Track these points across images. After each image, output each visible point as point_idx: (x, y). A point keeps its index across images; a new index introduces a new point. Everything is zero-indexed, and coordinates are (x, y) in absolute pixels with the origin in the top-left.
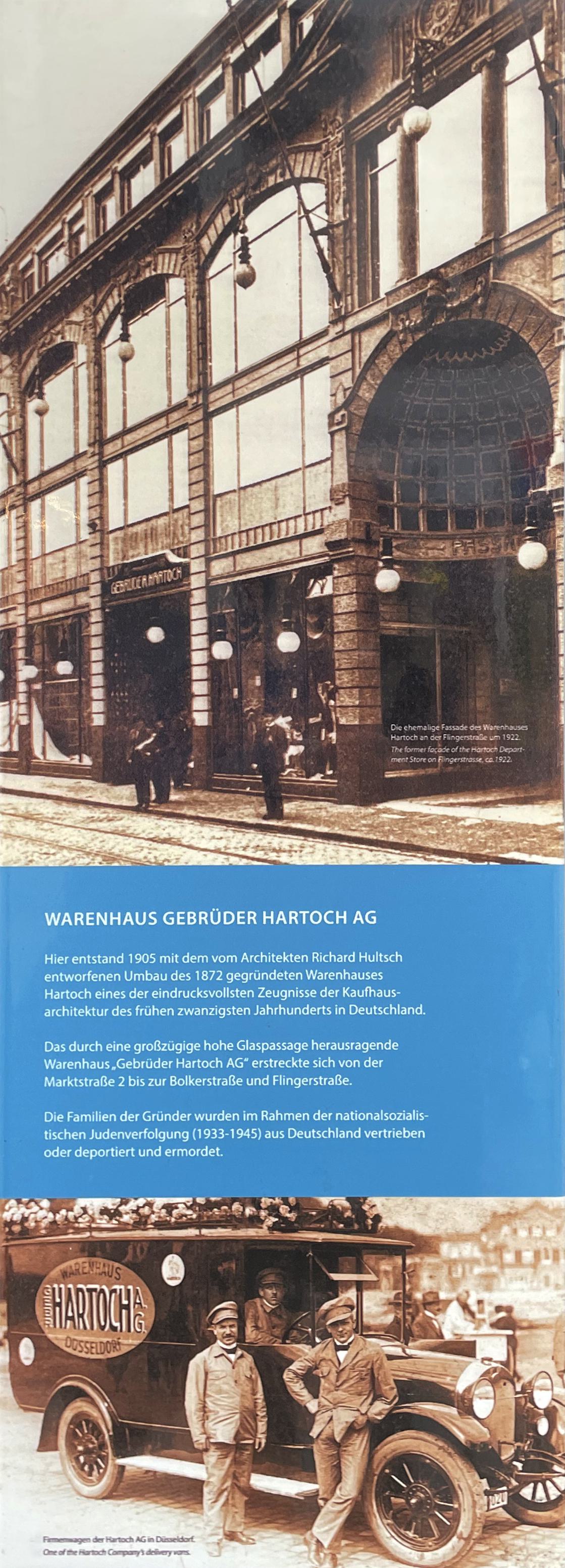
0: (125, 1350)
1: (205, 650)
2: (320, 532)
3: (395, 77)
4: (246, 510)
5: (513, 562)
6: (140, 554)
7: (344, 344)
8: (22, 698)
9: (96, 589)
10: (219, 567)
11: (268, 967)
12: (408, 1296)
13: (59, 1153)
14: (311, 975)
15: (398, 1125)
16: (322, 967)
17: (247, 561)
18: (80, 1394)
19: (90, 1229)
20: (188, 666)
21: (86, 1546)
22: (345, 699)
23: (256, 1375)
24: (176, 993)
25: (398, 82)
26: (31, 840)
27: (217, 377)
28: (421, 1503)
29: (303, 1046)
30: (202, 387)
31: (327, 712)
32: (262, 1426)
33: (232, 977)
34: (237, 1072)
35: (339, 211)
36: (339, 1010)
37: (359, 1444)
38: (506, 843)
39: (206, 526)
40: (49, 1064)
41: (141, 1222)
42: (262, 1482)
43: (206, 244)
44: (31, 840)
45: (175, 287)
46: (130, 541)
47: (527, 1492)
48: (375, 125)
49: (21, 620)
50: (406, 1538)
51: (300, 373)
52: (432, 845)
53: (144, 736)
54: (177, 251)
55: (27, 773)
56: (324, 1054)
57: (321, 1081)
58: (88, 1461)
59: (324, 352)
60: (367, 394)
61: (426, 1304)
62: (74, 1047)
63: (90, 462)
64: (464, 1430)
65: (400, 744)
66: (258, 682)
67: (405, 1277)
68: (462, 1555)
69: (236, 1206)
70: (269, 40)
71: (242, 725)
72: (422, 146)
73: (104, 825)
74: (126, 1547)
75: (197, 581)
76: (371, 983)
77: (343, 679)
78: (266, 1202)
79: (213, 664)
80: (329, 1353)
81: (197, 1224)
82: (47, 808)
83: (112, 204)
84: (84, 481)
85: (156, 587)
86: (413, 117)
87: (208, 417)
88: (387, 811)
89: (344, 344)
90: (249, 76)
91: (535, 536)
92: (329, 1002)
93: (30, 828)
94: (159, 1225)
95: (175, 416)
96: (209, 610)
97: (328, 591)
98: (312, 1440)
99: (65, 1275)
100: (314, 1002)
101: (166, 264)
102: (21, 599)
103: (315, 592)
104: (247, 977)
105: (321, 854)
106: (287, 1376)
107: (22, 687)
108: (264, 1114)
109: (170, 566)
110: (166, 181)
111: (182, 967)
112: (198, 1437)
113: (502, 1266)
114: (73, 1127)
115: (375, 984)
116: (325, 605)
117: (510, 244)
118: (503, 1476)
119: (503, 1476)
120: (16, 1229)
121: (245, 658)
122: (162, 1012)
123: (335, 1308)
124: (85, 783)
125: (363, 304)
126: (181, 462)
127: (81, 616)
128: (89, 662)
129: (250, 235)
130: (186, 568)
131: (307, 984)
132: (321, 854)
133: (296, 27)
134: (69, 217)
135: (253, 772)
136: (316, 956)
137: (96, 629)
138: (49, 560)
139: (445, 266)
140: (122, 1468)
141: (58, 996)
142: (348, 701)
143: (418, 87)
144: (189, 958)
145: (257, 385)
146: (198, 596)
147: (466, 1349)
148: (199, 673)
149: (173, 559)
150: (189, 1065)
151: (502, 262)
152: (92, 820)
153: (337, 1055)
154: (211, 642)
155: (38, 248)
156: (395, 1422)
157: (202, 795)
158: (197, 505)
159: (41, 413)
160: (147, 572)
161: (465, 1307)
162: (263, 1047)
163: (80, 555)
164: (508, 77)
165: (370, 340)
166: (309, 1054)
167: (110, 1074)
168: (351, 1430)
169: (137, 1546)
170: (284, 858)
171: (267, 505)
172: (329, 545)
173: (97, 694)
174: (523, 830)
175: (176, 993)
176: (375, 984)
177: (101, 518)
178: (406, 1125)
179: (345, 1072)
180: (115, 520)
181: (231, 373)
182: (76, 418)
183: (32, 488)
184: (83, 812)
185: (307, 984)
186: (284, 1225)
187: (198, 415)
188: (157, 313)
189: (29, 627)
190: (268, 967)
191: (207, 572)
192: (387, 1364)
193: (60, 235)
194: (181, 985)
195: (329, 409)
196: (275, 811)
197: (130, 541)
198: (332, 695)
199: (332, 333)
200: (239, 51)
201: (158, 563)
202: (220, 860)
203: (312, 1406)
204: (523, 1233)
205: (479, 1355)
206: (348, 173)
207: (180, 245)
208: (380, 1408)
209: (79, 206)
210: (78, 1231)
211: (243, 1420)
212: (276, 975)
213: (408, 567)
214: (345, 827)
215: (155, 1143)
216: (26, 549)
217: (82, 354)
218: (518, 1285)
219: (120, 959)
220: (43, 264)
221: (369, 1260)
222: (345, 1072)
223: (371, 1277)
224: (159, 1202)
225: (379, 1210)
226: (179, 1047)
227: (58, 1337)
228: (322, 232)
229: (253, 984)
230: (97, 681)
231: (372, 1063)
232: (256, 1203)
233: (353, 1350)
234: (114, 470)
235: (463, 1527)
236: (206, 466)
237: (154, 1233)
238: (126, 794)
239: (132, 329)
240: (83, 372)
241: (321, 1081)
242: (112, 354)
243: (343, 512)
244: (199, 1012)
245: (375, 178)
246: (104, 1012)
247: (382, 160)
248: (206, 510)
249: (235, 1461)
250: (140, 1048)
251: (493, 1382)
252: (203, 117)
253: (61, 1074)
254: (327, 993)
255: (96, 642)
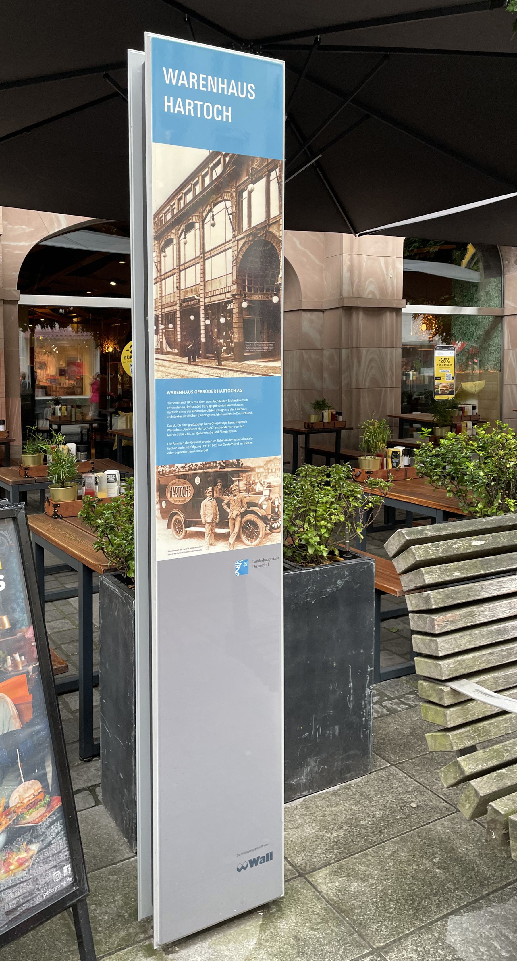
0: (187, 501)
1: (204, 322)
2: (230, 292)
3: (247, 176)
4: (213, 286)
5: (271, 301)
6: (188, 296)
7: (235, 243)
8: (161, 334)
9: (178, 305)
10: (207, 300)
11: (218, 404)
12: (249, 482)
13: (171, 453)
14: (228, 405)
15: (247, 441)
16: (230, 403)
17: (214, 299)
18: (177, 514)
19: (178, 472)
20: (200, 326)
21: (178, 552)
22: (236, 335)
23: (216, 505)
24: (197, 411)
25: (247, 177)
26: (163, 372)
27: (206, 250)
28: (252, 531)
29: (226, 423)
30: (203, 253)
31: (231, 338)
32: (218, 517)
33: (210, 406)
34: (212, 430)
35: (234, 209)
36: (234, 414)
37: (239, 518)
38: (270, 371)
39: (204, 289)
40: (168, 430)
41: (190, 469)
42: (218, 531)
43: (204, 215)
44: (163, 372)
45: (197, 225)
46: (186, 292)
47: (273, 526)
48: (242, 188)
49: (160, 313)
50: (248, 540)
51: (226, 250)
52: (254, 372)
53: (190, 344)
54: (197, 216)
55: (162, 354)
56: (231, 425)
57: (230, 431)
58: (179, 530)
59: (231, 245)
60: (240, 257)
61: (253, 484)
62: (174, 426)
63: (177, 271)
64: (261, 513)
65: (248, 347)
66: (216, 330)
67: (248, 477)
68: (260, 543)
69: (212, 463)
70: (218, 163)
71: (212, 342)
72: (252, 194)
73: (181, 368)
74: (187, 550)
75: (202, 304)
76: (241, 407)
77: (235, 330)
78: (218, 462)
79: (206, 326)
80: (232, 498)
81: (203, 469)
82: (167, 363)
83: (182, 202)
84: (175, 276)
85: (192, 305)
86: (251, 186)
87: (204, 260)
88: (245, 364)
89: (235, 243)
90: (214, 171)
91: (276, 295)
92: (232, 412)
93: (163, 369)
94: (195, 470)
95: (197, 260)
96: (205, 311)
97: (232, 307)
98: (229, 519)
99: (173, 484)
100: (229, 412)
101: (195, 219)
102: (160, 307)
103: (229, 308)
104: (214, 406)
105: (230, 375)
106: (223, 504)
107: (160, 331)
108: (218, 440)
109: (196, 299)
110: (195, 197)
111: (199, 404)
112: (204, 522)
113: (269, 473)
114: (174, 446)
115: (242, 407)
116: (231, 311)
117: (271, 221)
118: (268, 522)
119: (268, 522)
120: (161, 473)
121: (213, 324)
122: (195, 416)
123: (233, 487)
124: (176, 357)
125: (240, 234)
126: (198, 272)
127: (175, 312)
128: (177, 324)
129: (214, 213)
130: (199, 300)
131: (227, 407)
132: (230, 375)
133: (225, 160)
134: (172, 204)
135: (215, 354)
136: (229, 401)
137: (178, 316)
138: (167, 297)
139: (257, 225)
140: (186, 531)
141: (170, 412)
142: (236, 336)
143: (252, 179)
144: (201, 402)
145: (216, 253)
146: (202, 308)
147: (261, 493)
148: (202, 328)
149: (196, 297)
150: (201, 429)
151: (269, 225)
152: (178, 366)
153: (234, 425)
154: (205, 320)
155: (164, 212)
156: (247, 512)
157: (203, 360)
158: (202, 283)
159: (165, 257)
160: (191, 301)
161: (261, 483)
162: (217, 424)
163: (174, 296)
164: (271, 179)
165: (241, 243)
166: (228, 425)
167: (182, 432)
168: (237, 515)
169: (190, 550)
170: (222, 376)
171: (218, 284)
172: (232, 295)
173: (179, 333)
174: (273, 368)
175: (197, 411)
176: (242, 407)
177: (179, 286)
178: (248, 441)
179: (235, 429)
180: (183, 287)
181: (210, 249)
182: (173, 259)
183: (163, 277)
184: (176, 364)
185: (227, 407)
186: (222, 467)
187: (202, 260)
188: (193, 232)
189: (162, 315)
190: (218, 404)
191: (204, 301)
192: (245, 499)
193: (169, 209)
194: (199, 409)
195: (232, 260)
196: (220, 364)
197: (186, 292)
198: (232, 334)
199: (233, 241)
200: (212, 165)
201: (193, 299)
202: (207, 377)
203: (229, 511)
204: (273, 465)
205: (264, 494)
206: (236, 199)
207: (198, 214)
208: (243, 509)
209: (197, 179)
210: (176, 473)
211: (214, 515)
212: (220, 406)
213: (249, 301)
214: (235, 368)
215: (193, 449)
216: (161, 294)
217: (175, 241)
218: (272, 477)
219: (185, 403)
220: (165, 216)
221: (241, 474)
222: (235, 429)
223: (241, 478)
224: (194, 464)
225: (243, 462)
226: (198, 425)
227: (171, 500)
228: (231, 214)
229: (215, 408)
230: (179, 330)
231: (241, 426)
232: (216, 462)
233: (237, 496)
234: (182, 273)
235: (260, 536)
236: (204, 273)
237: (193, 472)
238: (186, 360)
239: (187, 236)
240: (175, 246)
241: (230, 431)
242: (182, 242)
243: (235, 287)
244: (203, 415)
245: (242, 201)
246: (181, 417)
247: (244, 197)
248: (204, 285)
249: (212, 526)
250: (190, 425)
251: (267, 501)
252: (203, 181)
253: (171, 433)
254: (232, 409)
255: (178, 319)
